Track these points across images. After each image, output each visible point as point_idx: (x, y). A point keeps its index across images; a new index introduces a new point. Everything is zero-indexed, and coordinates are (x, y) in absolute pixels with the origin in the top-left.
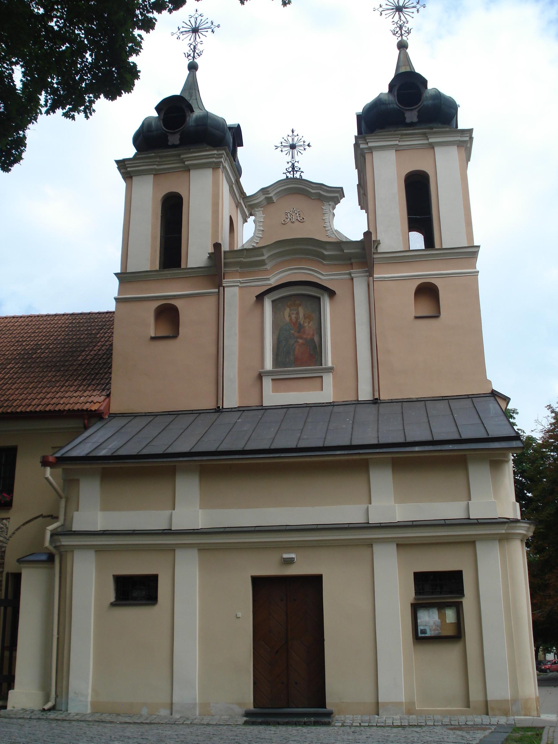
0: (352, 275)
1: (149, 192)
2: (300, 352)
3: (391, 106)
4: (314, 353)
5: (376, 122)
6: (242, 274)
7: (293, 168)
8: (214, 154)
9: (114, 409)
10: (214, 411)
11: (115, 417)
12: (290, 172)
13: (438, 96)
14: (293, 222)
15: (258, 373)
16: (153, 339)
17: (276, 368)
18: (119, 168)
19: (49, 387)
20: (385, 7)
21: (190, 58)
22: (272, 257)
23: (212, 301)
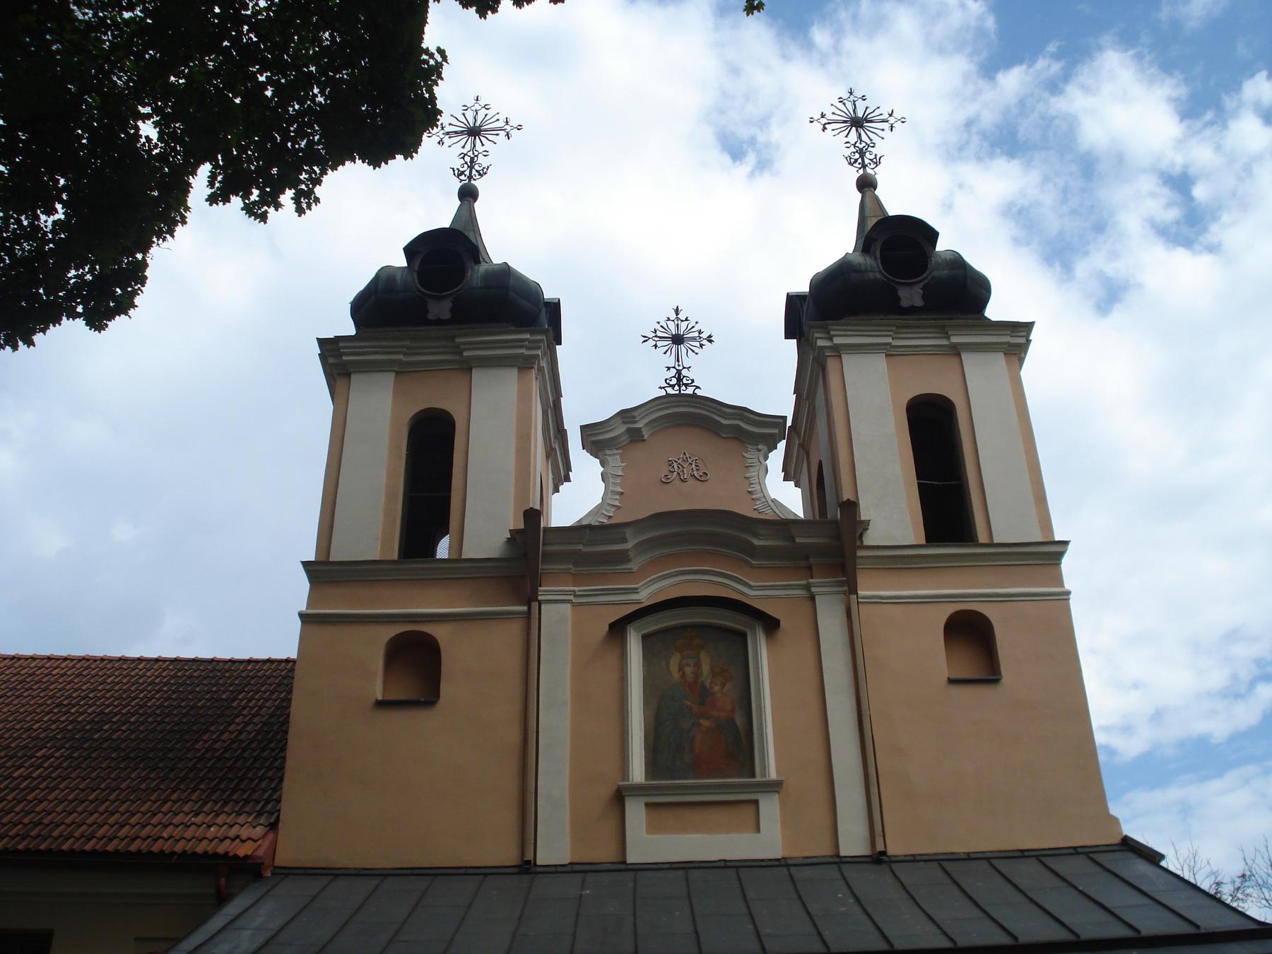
0: (813, 589)
1: (383, 407)
2: (705, 747)
3: (871, 275)
4: (735, 748)
5: (819, 314)
6: (577, 579)
7: (679, 379)
8: (525, 340)
9: (285, 857)
10: (516, 870)
11: (288, 875)
12: (673, 386)
13: (957, 263)
14: (684, 481)
15: (612, 790)
16: (381, 704)
17: (654, 779)
18: (323, 357)
19: (133, 802)
20: (829, 116)
21: (462, 177)
22: (644, 546)
23: (510, 633)
